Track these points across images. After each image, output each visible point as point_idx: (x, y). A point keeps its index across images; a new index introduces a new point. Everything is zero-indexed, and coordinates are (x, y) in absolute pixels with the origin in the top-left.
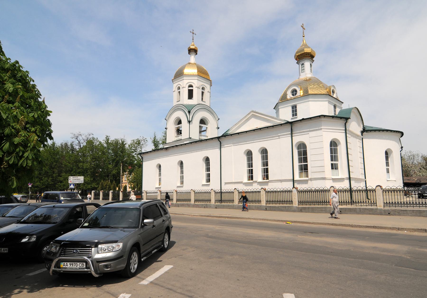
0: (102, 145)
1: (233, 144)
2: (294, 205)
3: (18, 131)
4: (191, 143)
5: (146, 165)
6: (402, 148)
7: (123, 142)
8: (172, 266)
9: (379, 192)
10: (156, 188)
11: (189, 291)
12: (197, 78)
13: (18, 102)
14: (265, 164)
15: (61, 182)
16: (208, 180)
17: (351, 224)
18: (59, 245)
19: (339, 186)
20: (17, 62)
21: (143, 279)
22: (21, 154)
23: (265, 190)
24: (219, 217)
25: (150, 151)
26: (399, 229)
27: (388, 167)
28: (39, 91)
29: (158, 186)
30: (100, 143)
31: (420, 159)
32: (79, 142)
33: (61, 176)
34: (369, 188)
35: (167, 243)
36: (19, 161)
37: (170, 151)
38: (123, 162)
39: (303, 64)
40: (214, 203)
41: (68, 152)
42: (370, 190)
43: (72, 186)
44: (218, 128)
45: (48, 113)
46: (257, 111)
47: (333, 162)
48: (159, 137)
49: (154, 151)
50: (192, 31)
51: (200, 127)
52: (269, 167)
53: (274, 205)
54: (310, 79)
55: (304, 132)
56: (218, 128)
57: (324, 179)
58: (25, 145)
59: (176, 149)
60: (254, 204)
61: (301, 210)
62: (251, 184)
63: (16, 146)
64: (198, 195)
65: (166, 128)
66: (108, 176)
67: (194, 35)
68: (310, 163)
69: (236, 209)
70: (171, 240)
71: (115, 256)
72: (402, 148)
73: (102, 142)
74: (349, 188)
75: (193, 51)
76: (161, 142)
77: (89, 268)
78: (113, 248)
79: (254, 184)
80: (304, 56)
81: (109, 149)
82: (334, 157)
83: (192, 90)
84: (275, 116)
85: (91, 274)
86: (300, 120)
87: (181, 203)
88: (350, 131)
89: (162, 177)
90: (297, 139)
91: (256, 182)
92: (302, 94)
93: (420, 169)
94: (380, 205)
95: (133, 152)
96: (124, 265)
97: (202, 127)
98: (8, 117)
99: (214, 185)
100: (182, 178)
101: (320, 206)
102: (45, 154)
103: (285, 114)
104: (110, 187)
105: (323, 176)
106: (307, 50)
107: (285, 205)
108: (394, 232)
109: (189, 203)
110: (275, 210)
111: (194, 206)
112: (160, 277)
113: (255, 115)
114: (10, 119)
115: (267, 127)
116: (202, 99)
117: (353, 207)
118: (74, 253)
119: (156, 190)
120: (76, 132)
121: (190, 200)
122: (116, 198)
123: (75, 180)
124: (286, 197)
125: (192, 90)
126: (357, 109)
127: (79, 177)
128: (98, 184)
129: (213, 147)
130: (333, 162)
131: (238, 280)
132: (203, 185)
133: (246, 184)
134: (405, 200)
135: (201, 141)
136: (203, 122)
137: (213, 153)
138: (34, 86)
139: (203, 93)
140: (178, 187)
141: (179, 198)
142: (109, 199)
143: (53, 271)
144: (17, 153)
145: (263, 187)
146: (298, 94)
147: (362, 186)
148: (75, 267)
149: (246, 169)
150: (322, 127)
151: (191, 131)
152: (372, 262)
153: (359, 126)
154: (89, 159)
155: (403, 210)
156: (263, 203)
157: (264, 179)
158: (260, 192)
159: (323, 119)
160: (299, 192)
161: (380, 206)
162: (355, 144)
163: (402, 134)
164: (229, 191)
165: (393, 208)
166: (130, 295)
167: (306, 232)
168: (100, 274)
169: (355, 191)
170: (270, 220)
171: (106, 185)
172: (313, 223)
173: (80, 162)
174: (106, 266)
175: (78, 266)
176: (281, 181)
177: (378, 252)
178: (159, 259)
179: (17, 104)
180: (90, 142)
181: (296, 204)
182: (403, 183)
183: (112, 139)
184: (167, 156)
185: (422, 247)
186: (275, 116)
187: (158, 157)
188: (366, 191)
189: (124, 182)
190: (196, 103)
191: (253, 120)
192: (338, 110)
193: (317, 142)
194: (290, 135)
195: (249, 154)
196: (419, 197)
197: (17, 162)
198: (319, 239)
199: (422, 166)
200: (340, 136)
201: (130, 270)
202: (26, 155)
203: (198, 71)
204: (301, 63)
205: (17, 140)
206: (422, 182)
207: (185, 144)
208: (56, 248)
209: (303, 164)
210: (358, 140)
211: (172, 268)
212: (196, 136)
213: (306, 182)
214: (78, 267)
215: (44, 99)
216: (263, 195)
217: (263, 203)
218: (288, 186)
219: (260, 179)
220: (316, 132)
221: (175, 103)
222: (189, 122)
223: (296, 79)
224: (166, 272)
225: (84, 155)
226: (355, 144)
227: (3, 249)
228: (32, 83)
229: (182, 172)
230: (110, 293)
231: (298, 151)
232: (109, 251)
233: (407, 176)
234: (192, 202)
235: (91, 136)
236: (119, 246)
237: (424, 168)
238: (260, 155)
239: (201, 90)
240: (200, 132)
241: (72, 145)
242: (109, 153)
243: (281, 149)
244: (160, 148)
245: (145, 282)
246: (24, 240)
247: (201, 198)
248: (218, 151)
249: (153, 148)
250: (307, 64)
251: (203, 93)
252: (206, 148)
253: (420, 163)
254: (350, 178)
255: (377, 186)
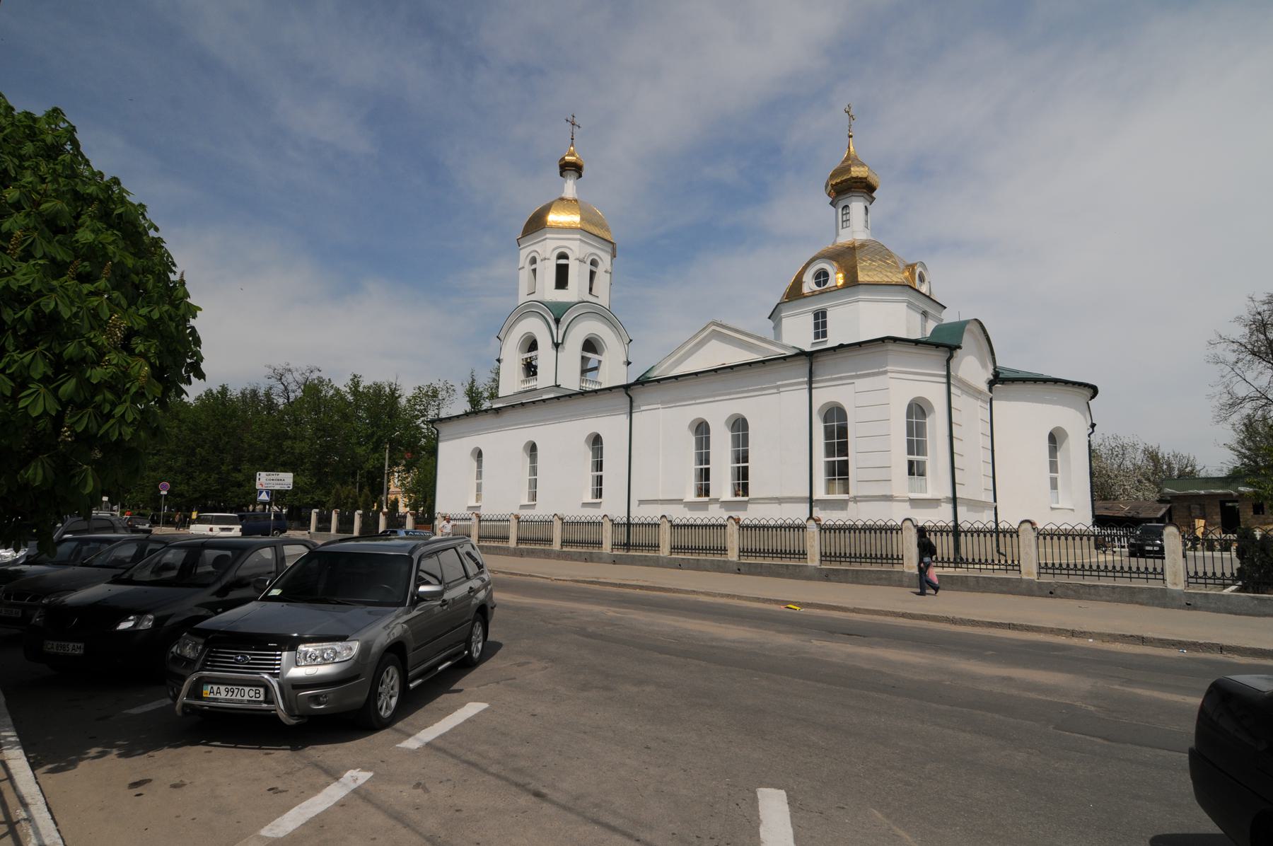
0: (342, 398)
1: (662, 403)
2: (810, 564)
3: (101, 353)
4: (558, 398)
5: (444, 448)
6: (1093, 426)
7: (393, 392)
8: (485, 706)
9: (1028, 536)
10: (469, 508)
11: (519, 771)
12: (578, 236)
13: (108, 280)
14: (742, 457)
15: (240, 485)
16: (599, 493)
17: (950, 616)
18: (202, 641)
19: (925, 518)
20: (116, 181)
21: (410, 735)
22: (107, 408)
23: (737, 521)
24: (620, 586)
25: (458, 417)
26: (1073, 634)
27: (1054, 475)
28: (169, 255)
29: (474, 504)
30: (337, 390)
31: (1140, 458)
32: (286, 388)
33: (239, 471)
34: (1001, 526)
35: (480, 646)
36: (100, 427)
37: (507, 416)
38: (391, 441)
39: (846, 207)
40: (609, 551)
41: (258, 412)
42: (1005, 532)
43: (264, 497)
44: (629, 363)
45: (193, 311)
46: (724, 323)
47: (912, 457)
48: (483, 382)
49: (467, 414)
50: (570, 118)
51: (584, 360)
52: (751, 464)
53: (760, 561)
54: (862, 245)
55: (841, 378)
56: (629, 363)
57: (888, 498)
58: (116, 385)
59: (520, 413)
60: (710, 557)
61: (827, 576)
62: (704, 506)
63: (97, 388)
64: (571, 528)
65: (499, 360)
66: (354, 475)
67: (576, 129)
68: (853, 459)
69: (663, 566)
70: (490, 638)
71: (339, 674)
72: (1093, 426)
73: (343, 389)
74: (951, 524)
75: (570, 168)
76: (486, 394)
77: (272, 703)
78: (336, 653)
79: (711, 507)
80: (849, 186)
81: (358, 407)
82: (916, 444)
83: (567, 266)
84: (771, 337)
85: (276, 716)
86: (834, 349)
87: (528, 546)
88: (960, 380)
89: (484, 481)
90: (824, 396)
91: (716, 500)
92: (840, 282)
93: (1139, 481)
94: (1029, 570)
95: (417, 417)
96: (361, 698)
97: (589, 359)
98: (76, 315)
99: (613, 506)
100: (534, 484)
101: (875, 568)
102: (203, 417)
103: (798, 332)
104: (356, 502)
105: (888, 494)
106: (856, 172)
107: (786, 562)
108: (1062, 640)
109: (547, 547)
110: (760, 574)
111: (561, 556)
112: (451, 730)
113: (720, 332)
114: (82, 320)
115: (750, 364)
116: (591, 289)
117: (960, 572)
118: (237, 662)
119: (468, 514)
120: (279, 364)
121: (550, 541)
122: (369, 531)
123: (271, 481)
124: (789, 541)
125: (567, 266)
126: (981, 324)
127: (282, 475)
128: (328, 493)
129: (612, 411)
130: (912, 457)
131: (647, 748)
132: (585, 505)
133: (691, 506)
134: (1094, 560)
135: (583, 393)
136: (590, 345)
137: (611, 426)
138: (157, 242)
139: (592, 274)
140: (523, 507)
141: (522, 535)
142: (329, 530)
143: (185, 705)
144: (98, 407)
145: (734, 514)
146: (830, 283)
147: (984, 519)
148: (239, 697)
149: (692, 467)
150: (889, 368)
151: (560, 369)
152: (997, 716)
153: (984, 366)
154: (309, 431)
155: (1089, 586)
156: (733, 556)
157: (736, 495)
158: (725, 526)
159: (891, 346)
160: (824, 529)
161: (1029, 573)
162: (970, 411)
163: (1094, 391)
164: (649, 520)
165: (1063, 579)
166: (370, 774)
167: (833, 633)
168: (300, 716)
169: (966, 533)
170: (747, 599)
171: (347, 497)
172: (854, 610)
173: (286, 436)
174: (315, 699)
175: (247, 696)
176: (780, 501)
177: (1015, 692)
178: (456, 687)
179: (102, 284)
180: (312, 389)
181: (813, 560)
182: (1094, 516)
183: (366, 382)
184: (499, 428)
185: (1130, 682)
186: (771, 337)
187: (477, 431)
188: (997, 532)
189: (392, 489)
190: (575, 299)
191: (714, 344)
192: (931, 325)
193: (875, 403)
194: (807, 386)
195: (702, 430)
196: (1132, 555)
197: (95, 429)
198: (864, 651)
199: (1143, 475)
200: (934, 392)
201: (377, 710)
202: (119, 411)
203: (582, 219)
204: (842, 204)
205: (97, 374)
206: (1142, 515)
207: (544, 401)
208: (194, 648)
209: (836, 459)
210: (979, 403)
211: (485, 710)
212: (572, 382)
213: (842, 505)
214: (246, 697)
215: (182, 275)
216: (732, 535)
217: (733, 556)
218: (798, 514)
219: (727, 495)
220: (871, 379)
221: (523, 298)
222: (557, 346)
223: (827, 245)
224: (469, 721)
225: (296, 420)
226: (970, 411)
227: (71, 645)
228: (152, 233)
229: (534, 471)
230: (321, 768)
231: (826, 427)
232: (325, 662)
233: (1105, 499)
234: (556, 546)
235: (315, 375)
236: (351, 649)
237: (1149, 480)
238: (730, 434)
239: (588, 267)
240: (584, 371)
241: (268, 395)
242: (359, 418)
243: (781, 421)
244: (483, 407)
245: (412, 744)
246: (124, 626)
247: (577, 537)
248: (624, 419)
249: (468, 407)
250: (857, 206)
251: (592, 274)
252: (596, 413)
253: (1140, 468)
254: (954, 500)
255: (1023, 522)
